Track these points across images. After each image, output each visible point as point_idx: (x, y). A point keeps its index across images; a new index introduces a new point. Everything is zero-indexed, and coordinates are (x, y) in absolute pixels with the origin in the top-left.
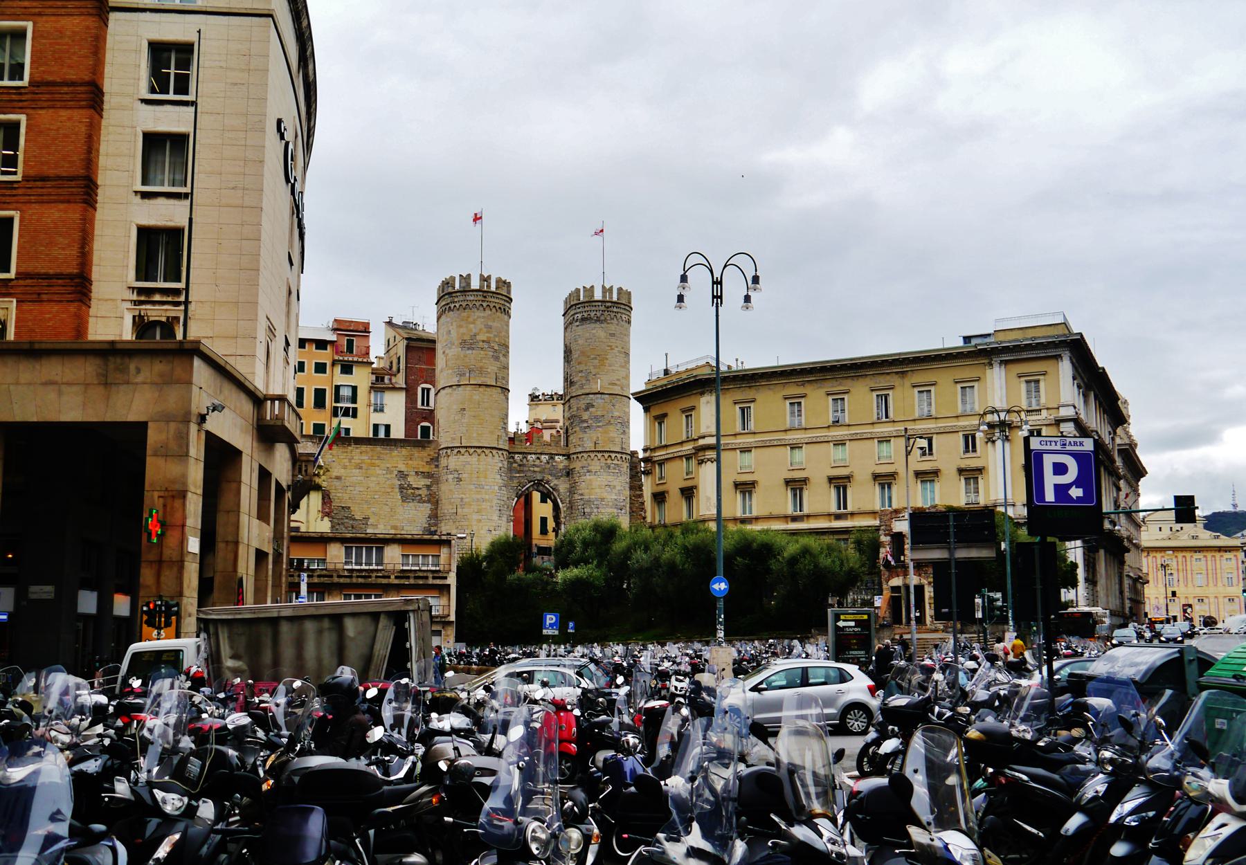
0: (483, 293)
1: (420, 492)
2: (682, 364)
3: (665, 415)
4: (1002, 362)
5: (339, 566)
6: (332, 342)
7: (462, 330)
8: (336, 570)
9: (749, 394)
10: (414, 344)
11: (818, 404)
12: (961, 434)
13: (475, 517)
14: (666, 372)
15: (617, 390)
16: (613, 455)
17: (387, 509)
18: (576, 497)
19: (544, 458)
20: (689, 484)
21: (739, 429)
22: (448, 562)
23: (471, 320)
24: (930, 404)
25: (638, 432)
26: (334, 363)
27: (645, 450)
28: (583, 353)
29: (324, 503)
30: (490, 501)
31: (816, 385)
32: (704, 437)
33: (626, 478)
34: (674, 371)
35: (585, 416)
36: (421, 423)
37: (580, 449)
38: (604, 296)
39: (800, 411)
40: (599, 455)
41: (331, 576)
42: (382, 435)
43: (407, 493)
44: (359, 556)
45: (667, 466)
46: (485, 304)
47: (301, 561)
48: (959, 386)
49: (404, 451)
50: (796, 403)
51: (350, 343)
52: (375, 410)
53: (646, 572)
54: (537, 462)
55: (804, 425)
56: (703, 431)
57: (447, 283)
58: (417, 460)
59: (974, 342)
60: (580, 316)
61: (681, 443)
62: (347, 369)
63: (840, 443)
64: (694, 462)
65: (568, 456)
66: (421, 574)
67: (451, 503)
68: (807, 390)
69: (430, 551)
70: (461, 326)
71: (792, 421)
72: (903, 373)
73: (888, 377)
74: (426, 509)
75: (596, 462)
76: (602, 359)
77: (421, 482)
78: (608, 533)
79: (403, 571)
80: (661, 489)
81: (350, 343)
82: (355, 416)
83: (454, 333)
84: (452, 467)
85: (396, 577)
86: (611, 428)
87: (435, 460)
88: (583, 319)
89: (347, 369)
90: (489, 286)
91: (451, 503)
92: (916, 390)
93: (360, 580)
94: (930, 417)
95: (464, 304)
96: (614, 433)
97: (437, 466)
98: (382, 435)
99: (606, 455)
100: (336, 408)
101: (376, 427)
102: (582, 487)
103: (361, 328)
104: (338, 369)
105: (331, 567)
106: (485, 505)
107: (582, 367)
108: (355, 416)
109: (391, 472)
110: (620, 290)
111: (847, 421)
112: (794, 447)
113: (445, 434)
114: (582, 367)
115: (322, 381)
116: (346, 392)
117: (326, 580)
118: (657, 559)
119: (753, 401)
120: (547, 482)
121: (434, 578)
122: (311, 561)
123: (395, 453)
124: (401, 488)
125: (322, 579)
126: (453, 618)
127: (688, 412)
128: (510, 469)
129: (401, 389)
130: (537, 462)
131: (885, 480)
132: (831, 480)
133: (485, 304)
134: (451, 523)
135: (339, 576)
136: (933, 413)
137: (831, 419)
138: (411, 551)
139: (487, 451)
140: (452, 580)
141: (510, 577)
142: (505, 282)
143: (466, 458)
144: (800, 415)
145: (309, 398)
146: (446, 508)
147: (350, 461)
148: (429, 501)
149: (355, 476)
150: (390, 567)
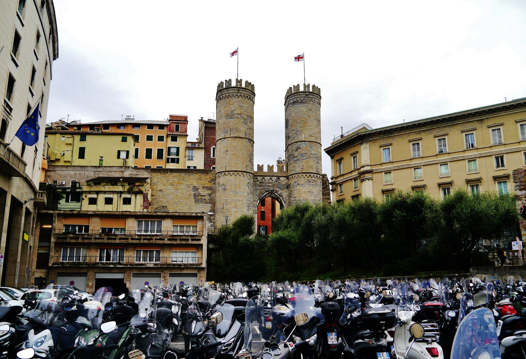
0: (238, 88)
1: (205, 198)
2: (350, 131)
3: (342, 159)
5: (133, 233)
6: (167, 125)
7: (226, 109)
8: (130, 235)
10: (209, 125)
11: (429, 143)
12: (522, 152)
13: (234, 210)
15: (313, 139)
16: (312, 175)
18: (292, 199)
19: (274, 179)
20: (356, 193)
22: (203, 230)
23: (231, 103)
24: (500, 137)
25: (327, 166)
27: (332, 178)
28: (294, 120)
29: (144, 201)
30: (242, 201)
31: (427, 133)
32: (363, 167)
33: (320, 188)
34: (346, 135)
35: (296, 154)
36: (209, 162)
37: (293, 172)
38: (305, 89)
39: (418, 148)
40: (304, 175)
41: (128, 239)
43: (198, 198)
44: (147, 226)
45: (344, 186)
46: (239, 94)
47: (110, 230)
48: (519, 124)
50: (416, 144)
51: (177, 127)
52: (189, 160)
53: (324, 229)
54: (270, 181)
55: (421, 156)
56: (363, 163)
57: (220, 85)
58: (205, 180)
60: (292, 101)
61: (351, 172)
62: (174, 139)
63: (445, 164)
64: (358, 181)
65: (287, 177)
66: (184, 238)
67: (221, 203)
68: (423, 135)
69: (191, 223)
70: (226, 107)
71: (414, 154)
72: (481, 120)
73: (472, 124)
76: (304, 123)
78: (303, 210)
79: (173, 236)
80: (341, 198)
81: (177, 127)
83: (222, 112)
84: (221, 183)
85: (168, 240)
86: (310, 160)
87: (213, 180)
88: (294, 103)
89: (174, 139)
90: (241, 85)
91: (221, 203)
92: (490, 129)
93: (146, 241)
94: (501, 144)
95: (227, 95)
96: (312, 162)
97: (215, 184)
99: (308, 175)
100: (168, 159)
102: (295, 193)
103: (183, 119)
104: (170, 139)
105: (127, 233)
106: (239, 203)
107: (294, 128)
108: (178, 162)
110: (314, 86)
111: (448, 151)
112: (416, 168)
113: (219, 167)
114: (294, 128)
115: (149, 145)
116: (173, 150)
117: (124, 241)
118: (331, 219)
120: (276, 192)
121: (192, 240)
122: (117, 229)
123: (192, 177)
124: (195, 195)
125: (122, 241)
126: (204, 265)
127: (354, 155)
128: (255, 185)
129: (202, 148)
132: (440, 185)
133: (239, 94)
134: (221, 214)
135: (132, 239)
136: (503, 141)
138: (180, 223)
139: (240, 173)
140: (204, 241)
141: (242, 239)
143: (229, 177)
144: (419, 150)
145: (155, 154)
146: (218, 206)
147: (167, 182)
148: (210, 203)
149: (170, 189)
150: (164, 233)
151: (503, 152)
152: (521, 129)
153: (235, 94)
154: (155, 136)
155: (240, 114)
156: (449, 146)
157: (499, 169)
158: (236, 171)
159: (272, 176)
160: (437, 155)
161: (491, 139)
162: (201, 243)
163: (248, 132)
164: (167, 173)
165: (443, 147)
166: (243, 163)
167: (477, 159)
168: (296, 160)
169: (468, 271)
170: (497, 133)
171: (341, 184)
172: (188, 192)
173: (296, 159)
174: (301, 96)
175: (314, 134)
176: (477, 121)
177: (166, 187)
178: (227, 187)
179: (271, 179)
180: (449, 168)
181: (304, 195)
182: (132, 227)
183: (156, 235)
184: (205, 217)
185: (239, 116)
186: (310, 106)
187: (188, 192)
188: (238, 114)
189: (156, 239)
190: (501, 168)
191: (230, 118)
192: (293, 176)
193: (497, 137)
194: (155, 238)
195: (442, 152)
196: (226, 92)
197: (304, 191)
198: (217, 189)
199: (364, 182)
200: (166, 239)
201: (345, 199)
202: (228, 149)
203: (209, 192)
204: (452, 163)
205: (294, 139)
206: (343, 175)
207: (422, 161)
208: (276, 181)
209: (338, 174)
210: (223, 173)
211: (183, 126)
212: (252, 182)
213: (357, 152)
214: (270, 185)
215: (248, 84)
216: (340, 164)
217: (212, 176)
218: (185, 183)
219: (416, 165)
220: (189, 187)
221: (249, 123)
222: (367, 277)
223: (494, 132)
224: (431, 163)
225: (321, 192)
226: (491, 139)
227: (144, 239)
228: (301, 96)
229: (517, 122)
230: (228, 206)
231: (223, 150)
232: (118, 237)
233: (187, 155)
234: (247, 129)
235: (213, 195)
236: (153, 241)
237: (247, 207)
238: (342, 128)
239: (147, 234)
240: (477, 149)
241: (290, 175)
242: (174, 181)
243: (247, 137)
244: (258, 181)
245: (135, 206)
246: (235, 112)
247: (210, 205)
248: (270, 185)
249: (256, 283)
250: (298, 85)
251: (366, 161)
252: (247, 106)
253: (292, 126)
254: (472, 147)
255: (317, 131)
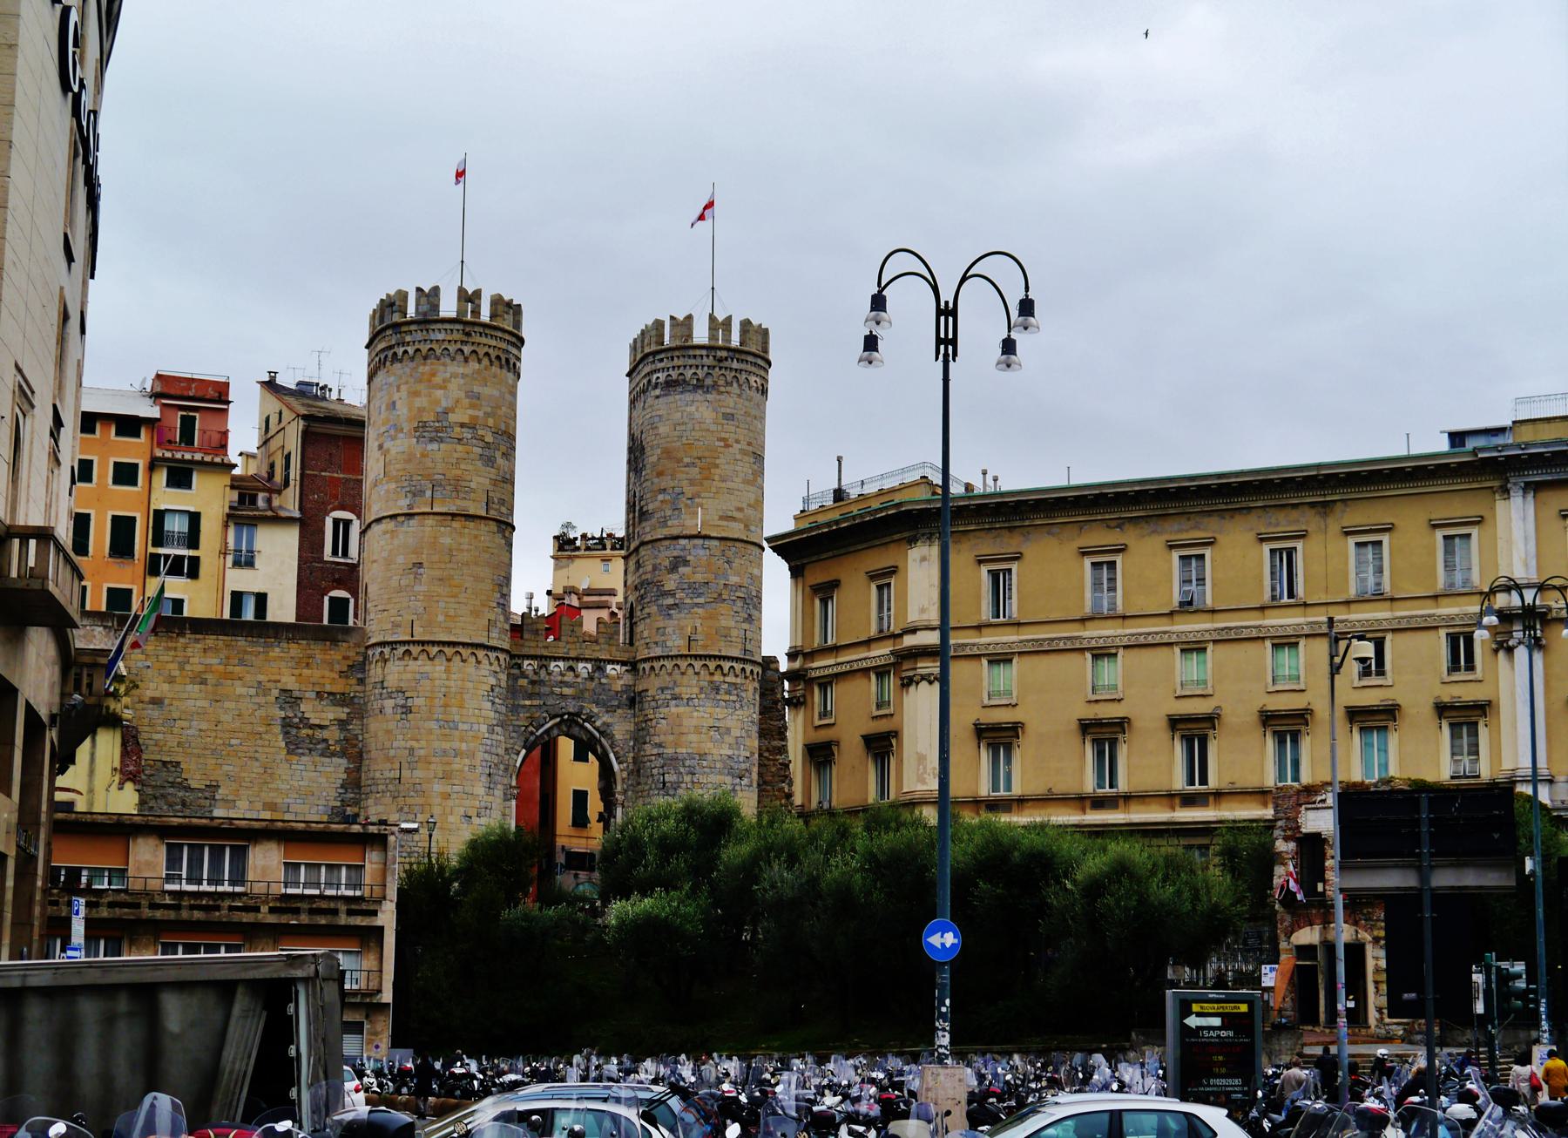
0: (465, 325)
1: (325, 734)
3: (835, 584)
4: (1529, 487)
5: (154, 885)
6: (150, 422)
7: (420, 402)
8: (147, 893)
9: (1010, 544)
10: (318, 428)
11: (1150, 565)
12: (1443, 633)
13: (438, 787)
14: (839, 495)
15: (735, 530)
16: (726, 665)
17: (256, 768)
18: (649, 749)
19: (584, 668)
20: (883, 726)
21: (986, 614)
22: (381, 881)
23: (438, 379)
24: (1380, 570)
26: (153, 465)
27: (792, 656)
28: (668, 453)
29: (125, 754)
32: (913, 631)
33: (751, 713)
34: (854, 493)
35: (670, 583)
37: (658, 652)
38: (713, 337)
39: (1112, 580)
40: (698, 664)
42: (249, 614)
43: (299, 737)
44: (195, 864)
45: (837, 692)
46: (467, 349)
47: (74, 874)
48: (1439, 534)
49: (295, 650)
51: (188, 424)
52: (237, 564)
54: (569, 677)
55: (1120, 609)
56: (913, 617)
59: (1471, 444)
60: (662, 376)
61: (868, 643)
62: (180, 477)
63: (1194, 648)
64: (892, 682)
65: (633, 666)
66: (324, 905)
67: (389, 759)
69: (344, 857)
70: (416, 394)
71: (1097, 602)
72: (1325, 504)
73: (1294, 514)
74: (337, 769)
75: (690, 679)
76: (707, 465)
77: (329, 714)
79: (286, 897)
81: (188, 424)
82: (194, 573)
83: (402, 410)
85: (272, 910)
86: (723, 608)
87: (358, 668)
88: (670, 384)
89: (180, 477)
90: (476, 312)
91: (389, 759)
93: (198, 915)
94: (1379, 597)
95: (424, 348)
96: (728, 619)
97: (361, 682)
98: (249, 614)
99: (712, 665)
101: (237, 597)
103: (211, 393)
104: (161, 477)
105: (137, 886)
106: (459, 764)
107: (666, 482)
108: (194, 573)
109: (266, 692)
112: (1102, 653)
114: (666, 482)
116: (176, 525)
117: (125, 913)
118: (814, 881)
119: (1017, 557)
120: (589, 719)
121: (350, 913)
123: (276, 652)
124: (287, 724)
126: (387, 997)
127: (884, 577)
128: (513, 691)
129: (290, 520)
130: (569, 677)
131: (1286, 726)
132: (1175, 722)
133: (467, 349)
134: (388, 799)
137: (1176, 598)
139: (465, 652)
142: (509, 304)
144: (1112, 589)
145: (100, 536)
146: (379, 769)
147: (182, 669)
148: (343, 754)
149: (193, 698)
150: (259, 888)
151: (1385, 625)
152: (1446, 552)
153: (452, 348)
154: (103, 465)
155: (471, 426)
156: (1214, 585)
157: (1366, 682)
158: (449, 644)
159: (578, 659)
160: (1171, 614)
161: (1352, 575)
162: (379, 923)
163: (496, 496)
164: (182, 634)
165: (1193, 587)
166: (476, 614)
167: (1302, 642)
168: (670, 607)
169: (1128, 1039)
170: (1370, 556)
171: (825, 683)
172: (261, 713)
173: (670, 601)
174: (698, 361)
175: (740, 509)
176: (1312, 505)
177: (177, 687)
178: (419, 702)
179: (571, 669)
180: (1209, 665)
181: (693, 737)
182: (148, 864)
183: (233, 895)
184: (392, 839)
185: (467, 434)
186: (730, 401)
187: (261, 713)
188: (462, 425)
189: (231, 908)
190: (1374, 680)
191: (432, 440)
192: (657, 665)
193: (1371, 569)
194: (227, 903)
195: (1190, 603)
196: (419, 336)
197: (694, 722)
198: (376, 705)
199: (912, 688)
200: (264, 909)
201: (838, 743)
202: (424, 558)
203: (342, 713)
204: (1220, 647)
205: (664, 524)
206: (836, 649)
207: (1120, 631)
208: (591, 678)
209: (817, 642)
210: (402, 649)
211: (213, 424)
212: (503, 684)
213: (893, 571)
214: (566, 691)
215: (500, 308)
216: (824, 602)
217: (351, 654)
218: (248, 678)
219: (1101, 643)
220: (266, 692)
221: (500, 461)
222: (903, 1045)
223: (1363, 550)
224: (1150, 640)
225: (755, 728)
226: (1352, 575)
227: (192, 907)
228: (698, 361)
229: (1435, 526)
230: (419, 774)
231: (400, 559)
232: (105, 900)
233: (231, 545)
234: (495, 482)
235: (354, 727)
236: (221, 915)
237: (484, 779)
238: (839, 460)
239: (220, 889)
240: (1305, 605)
241: (645, 660)
242: (208, 668)
243: (493, 514)
244: (524, 675)
245: (92, 772)
246: (452, 417)
247: (344, 761)
248: (566, 691)
249: (822, 1060)
250: (689, 318)
251: (923, 610)
252: (496, 393)
253: (660, 474)
254: (1291, 595)
255: (752, 497)
